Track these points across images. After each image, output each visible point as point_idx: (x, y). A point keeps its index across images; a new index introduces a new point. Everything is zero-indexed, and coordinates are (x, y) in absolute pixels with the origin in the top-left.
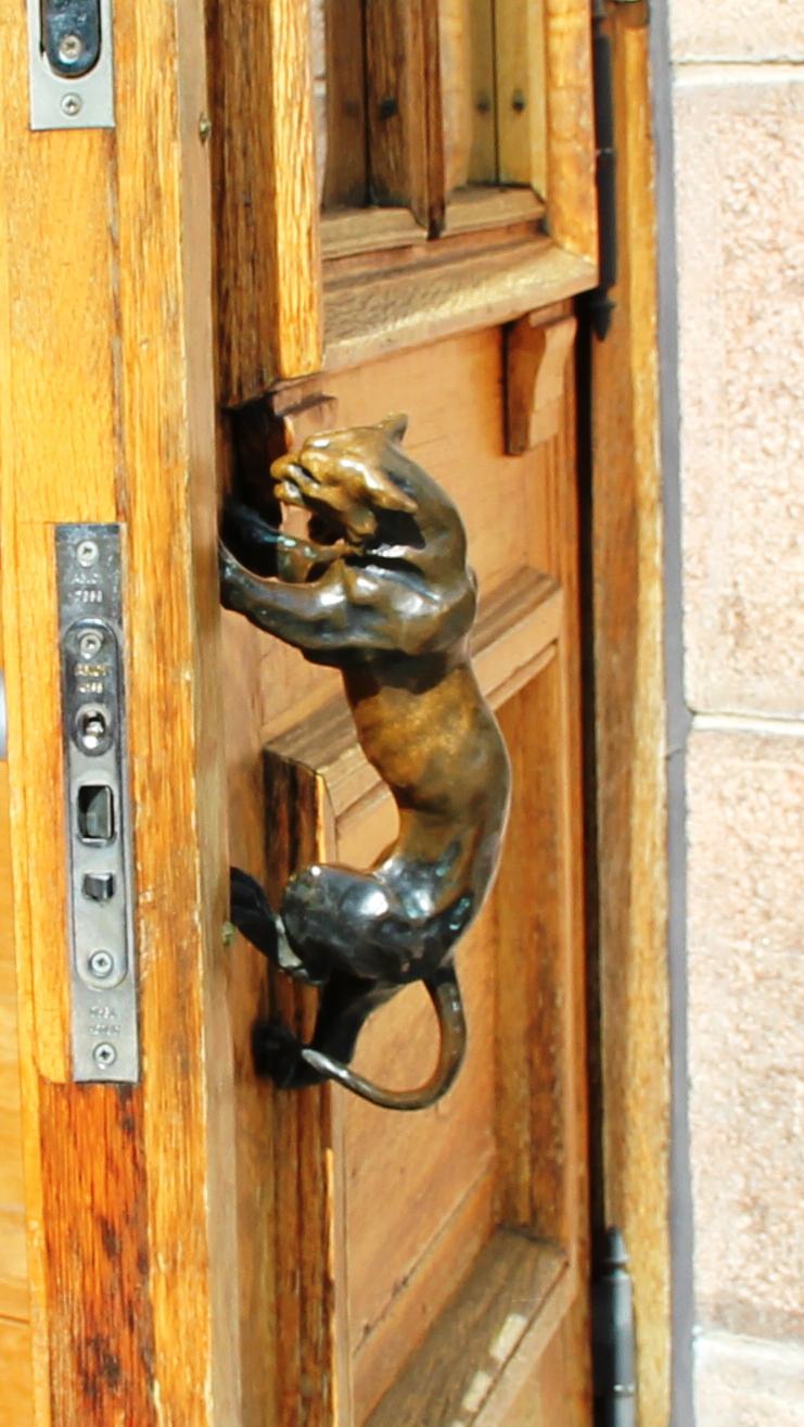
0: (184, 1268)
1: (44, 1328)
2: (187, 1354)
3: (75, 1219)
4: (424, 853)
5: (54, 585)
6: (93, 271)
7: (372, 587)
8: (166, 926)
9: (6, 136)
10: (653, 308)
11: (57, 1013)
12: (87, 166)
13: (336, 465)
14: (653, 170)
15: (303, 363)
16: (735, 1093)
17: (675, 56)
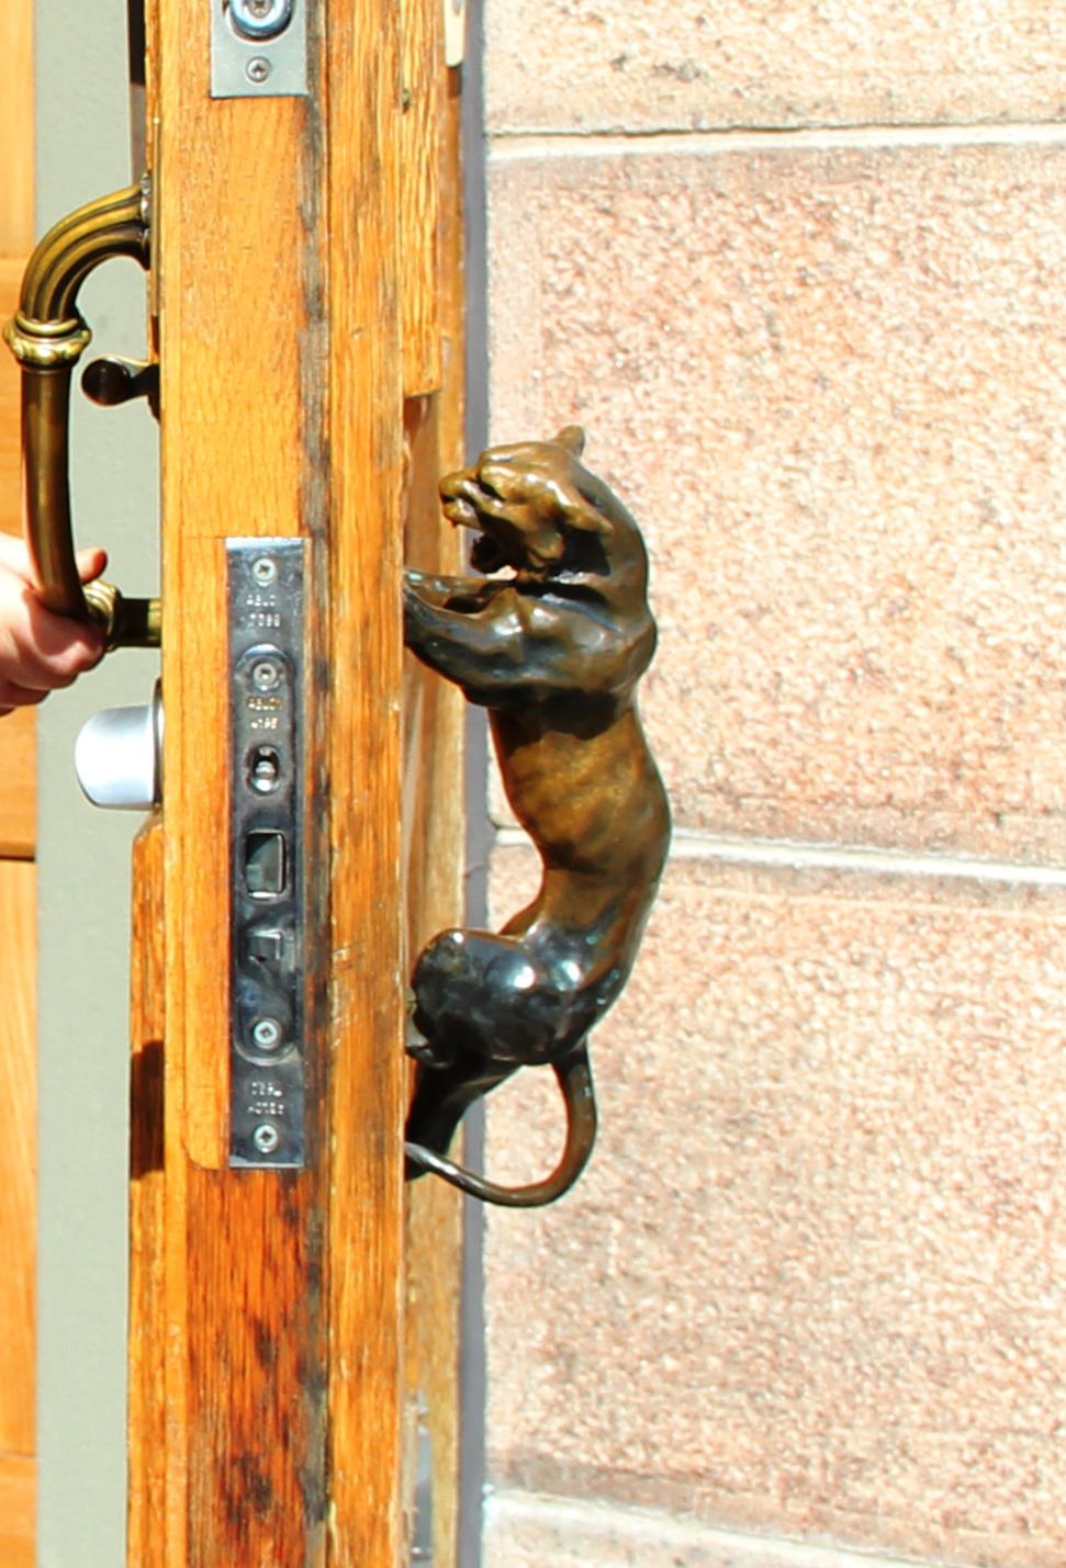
0: (370, 1374)
1: (183, 1448)
2: (370, 1472)
3: (224, 1322)
4: (573, 918)
5: (224, 608)
6: (279, 257)
7: (553, 618)
8: (363, 990)
9: (181, 104)
10: (460, 396)
11: (211, 1090)
12: (275, 140)
13: (524, 480)
14: (462, 248)
15: (425, 380)
16: (538, 1233)
17: (490, 128)
